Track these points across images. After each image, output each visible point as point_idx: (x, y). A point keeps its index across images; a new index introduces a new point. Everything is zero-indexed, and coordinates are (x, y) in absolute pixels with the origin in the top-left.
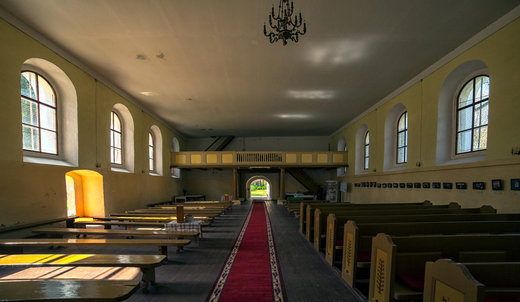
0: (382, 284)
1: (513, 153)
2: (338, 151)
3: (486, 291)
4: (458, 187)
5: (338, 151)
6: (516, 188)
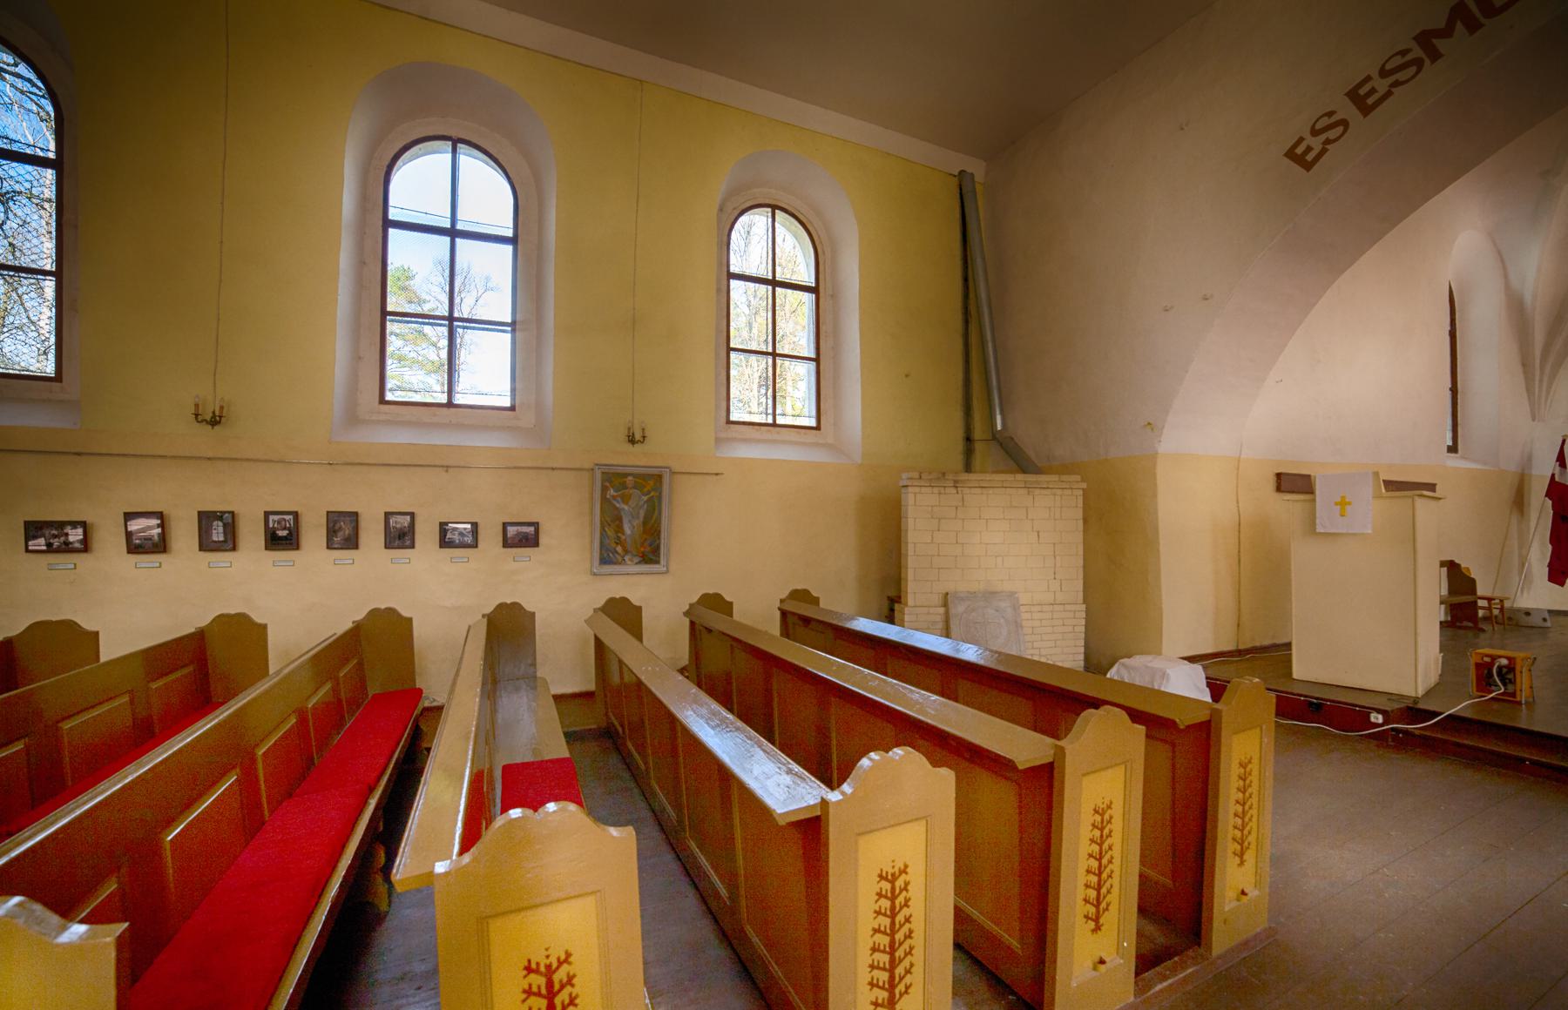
0: (1092, 894)
1: (200, 418)
2: (731, 280)
3: (170, 838)
4: (445, 540)
5: (731, 280)
6: (215, 542)
